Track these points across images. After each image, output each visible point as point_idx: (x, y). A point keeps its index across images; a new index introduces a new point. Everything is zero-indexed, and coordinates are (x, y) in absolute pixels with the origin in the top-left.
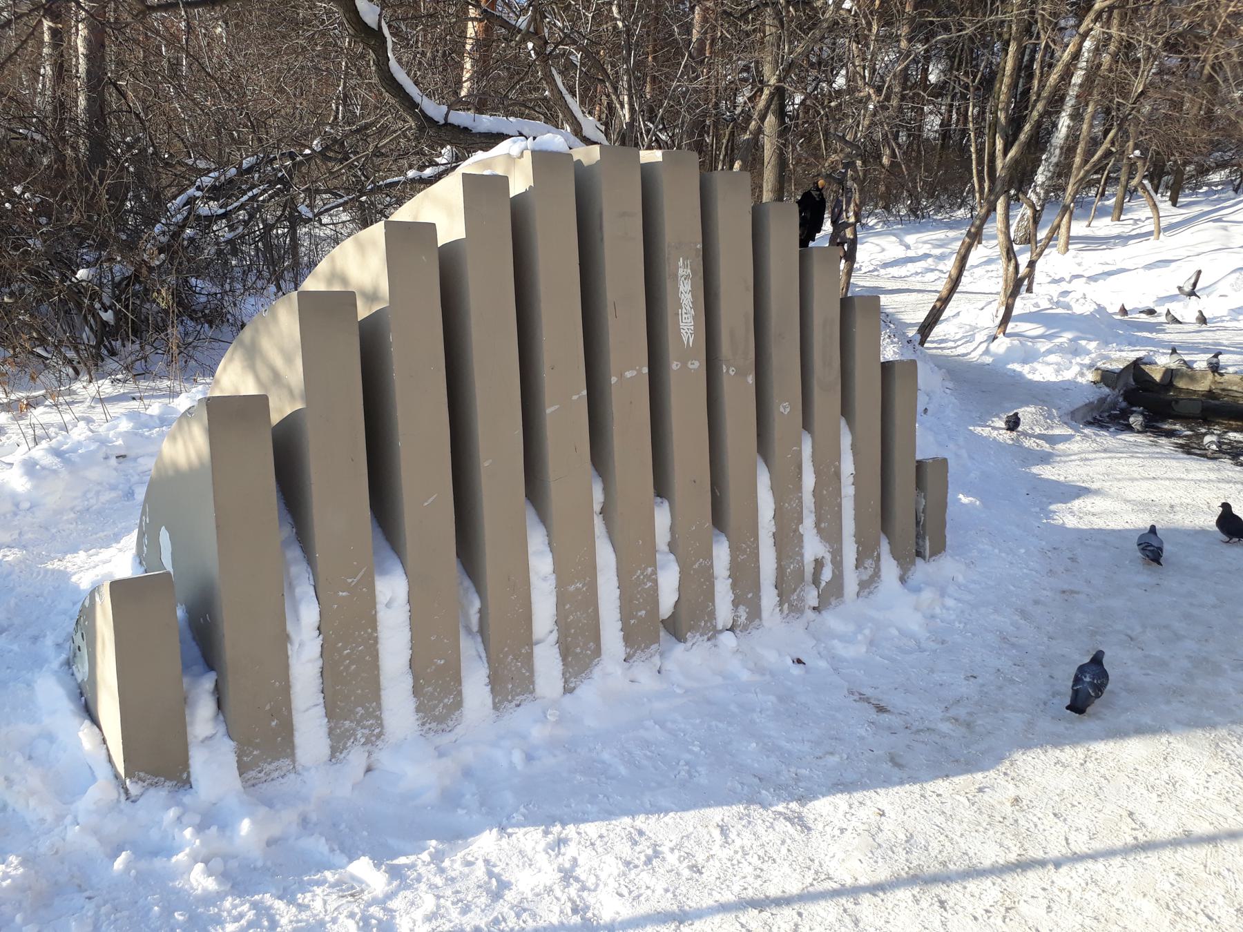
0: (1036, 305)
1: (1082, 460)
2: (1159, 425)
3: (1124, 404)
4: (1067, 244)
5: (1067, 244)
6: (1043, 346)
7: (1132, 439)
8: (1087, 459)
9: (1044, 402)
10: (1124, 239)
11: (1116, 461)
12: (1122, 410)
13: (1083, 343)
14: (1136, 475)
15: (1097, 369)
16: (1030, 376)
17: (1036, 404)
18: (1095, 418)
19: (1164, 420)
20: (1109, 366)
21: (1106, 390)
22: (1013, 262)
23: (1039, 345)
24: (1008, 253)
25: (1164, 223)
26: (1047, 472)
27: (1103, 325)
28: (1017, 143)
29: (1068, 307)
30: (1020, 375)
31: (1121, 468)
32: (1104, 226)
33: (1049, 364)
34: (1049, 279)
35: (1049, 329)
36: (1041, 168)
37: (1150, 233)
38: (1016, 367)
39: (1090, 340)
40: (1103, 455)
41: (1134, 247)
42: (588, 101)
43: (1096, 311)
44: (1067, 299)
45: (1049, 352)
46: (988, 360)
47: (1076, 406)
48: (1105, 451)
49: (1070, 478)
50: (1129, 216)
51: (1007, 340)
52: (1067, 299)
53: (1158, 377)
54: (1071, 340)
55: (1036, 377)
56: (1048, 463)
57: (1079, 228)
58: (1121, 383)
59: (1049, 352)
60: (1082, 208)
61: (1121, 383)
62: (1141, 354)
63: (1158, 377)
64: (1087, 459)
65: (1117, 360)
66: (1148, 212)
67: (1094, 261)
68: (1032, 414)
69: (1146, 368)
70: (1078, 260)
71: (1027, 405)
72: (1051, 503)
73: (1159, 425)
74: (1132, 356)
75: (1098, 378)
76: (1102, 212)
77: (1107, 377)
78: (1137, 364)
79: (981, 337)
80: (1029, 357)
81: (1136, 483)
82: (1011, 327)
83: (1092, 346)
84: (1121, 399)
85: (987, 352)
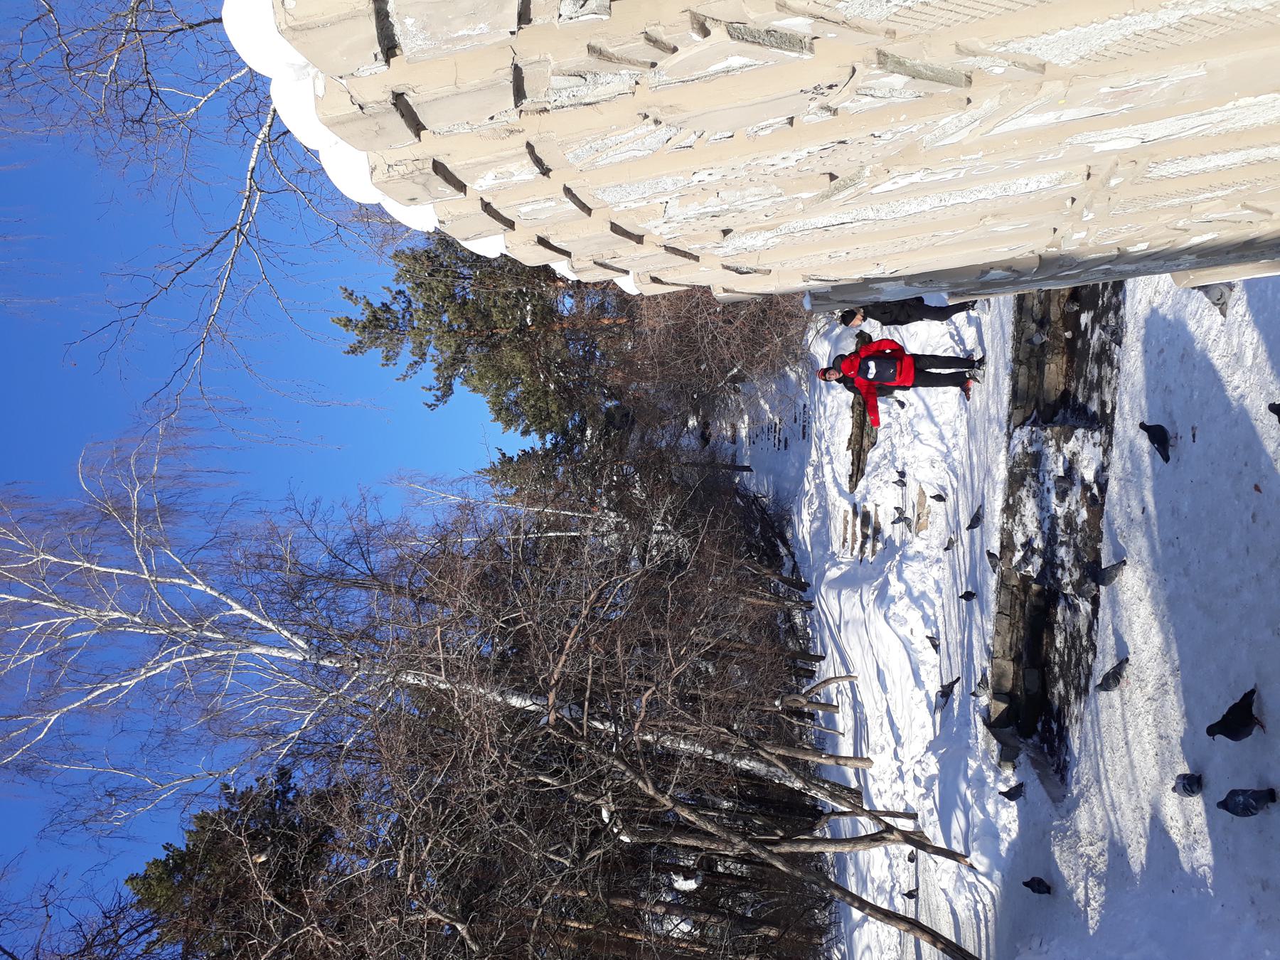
0: (930, 812)
1: (1114, 810)
2: (1055, 708)
3: (1036, 738)
4: (862, 759)
5: (862, 759)
6: (977, 815)
7: (1077, 741)
8: (1113, 804)
9: (1046, 833)
10: (857, 705)
11: (1110, 775)
12: (1043, 740)
13: (970, 772)
14: (1126, 760)
15: (999, 765)
16: (1014, 835)
17: (1049, 844)
18: (1056, 772)
19: (1050, 703)
20: (995, 754)
21: (1022, 757)
22: (885, 835)
23: (976, 820)
24: (876, 840)
25: (844, 674)
26: (1138, 854)
27: (949, 745)
28: (770, 861)
29: (931, 779)
30: (1012, 845)
31: (1120, 771)
32: (844, 720)
33: (997, 812)
34: (899, 781)
35: (957, 805)
36: (787, 783)
37: (852, 684)
38: (1004, 847)
39: (967, 765)
40: (1104, 786)
41: (865, 696)
42: (673, 646)
43: (934, 753)
44: (923, 779)
45: (983, 810)
46: (997, 875)
47: (1045, 794)
48: (1098, 782)
49: (1140, 830)
50: (834, 696)
51: (973, 855)
52: (923, 779)
53: (1003, 706)
54: (969, 786)
55: (1015, 827)
56: (1125, 851)
57: (846, 748)
58: (1011, 742)
59: (983, 810)
60: (824, 744)
61: (1011, 742)
62: (979, 719)
63: (1003, 706)
64: (1113, 804)
65: (988, 744)
66: (832, 687)
67: (878, 734)
68: (1062, 852)
69: (994, 716)
70: (878, 749)
71: (1052, 854)
72: (1181, 869)
73: (1055, 708)
74: (981, 729)
75: (1009, 764)
76: (831, 722)
77: (1008, 756)
78: (988, 724)
79: (971, 878)
80: (991, 832)
81: (1136, 763)
82: (958, 847)
83: (973, 764)
84: (1030, 741)
85: (988, 876)
